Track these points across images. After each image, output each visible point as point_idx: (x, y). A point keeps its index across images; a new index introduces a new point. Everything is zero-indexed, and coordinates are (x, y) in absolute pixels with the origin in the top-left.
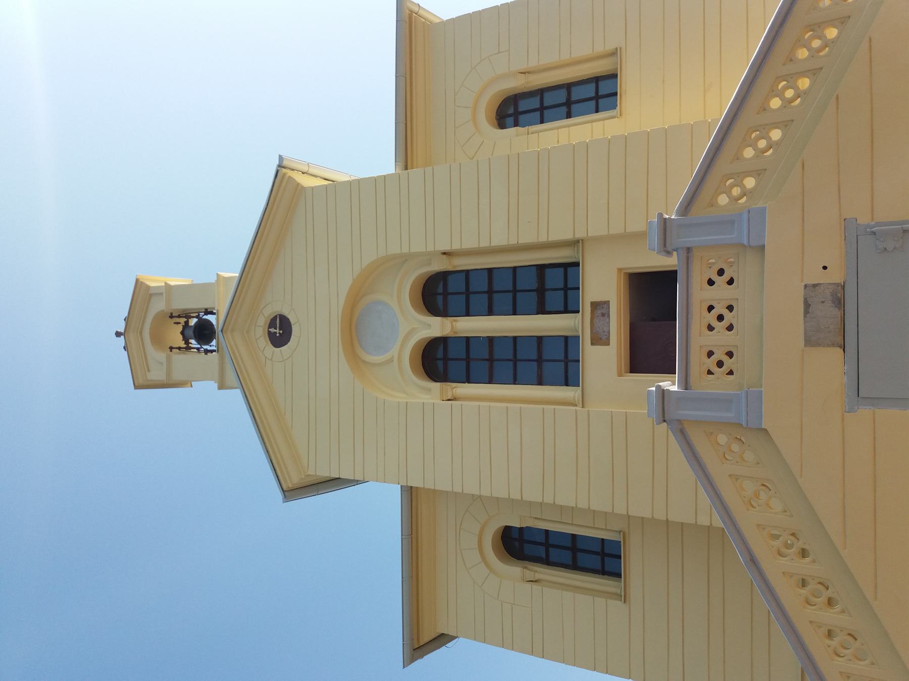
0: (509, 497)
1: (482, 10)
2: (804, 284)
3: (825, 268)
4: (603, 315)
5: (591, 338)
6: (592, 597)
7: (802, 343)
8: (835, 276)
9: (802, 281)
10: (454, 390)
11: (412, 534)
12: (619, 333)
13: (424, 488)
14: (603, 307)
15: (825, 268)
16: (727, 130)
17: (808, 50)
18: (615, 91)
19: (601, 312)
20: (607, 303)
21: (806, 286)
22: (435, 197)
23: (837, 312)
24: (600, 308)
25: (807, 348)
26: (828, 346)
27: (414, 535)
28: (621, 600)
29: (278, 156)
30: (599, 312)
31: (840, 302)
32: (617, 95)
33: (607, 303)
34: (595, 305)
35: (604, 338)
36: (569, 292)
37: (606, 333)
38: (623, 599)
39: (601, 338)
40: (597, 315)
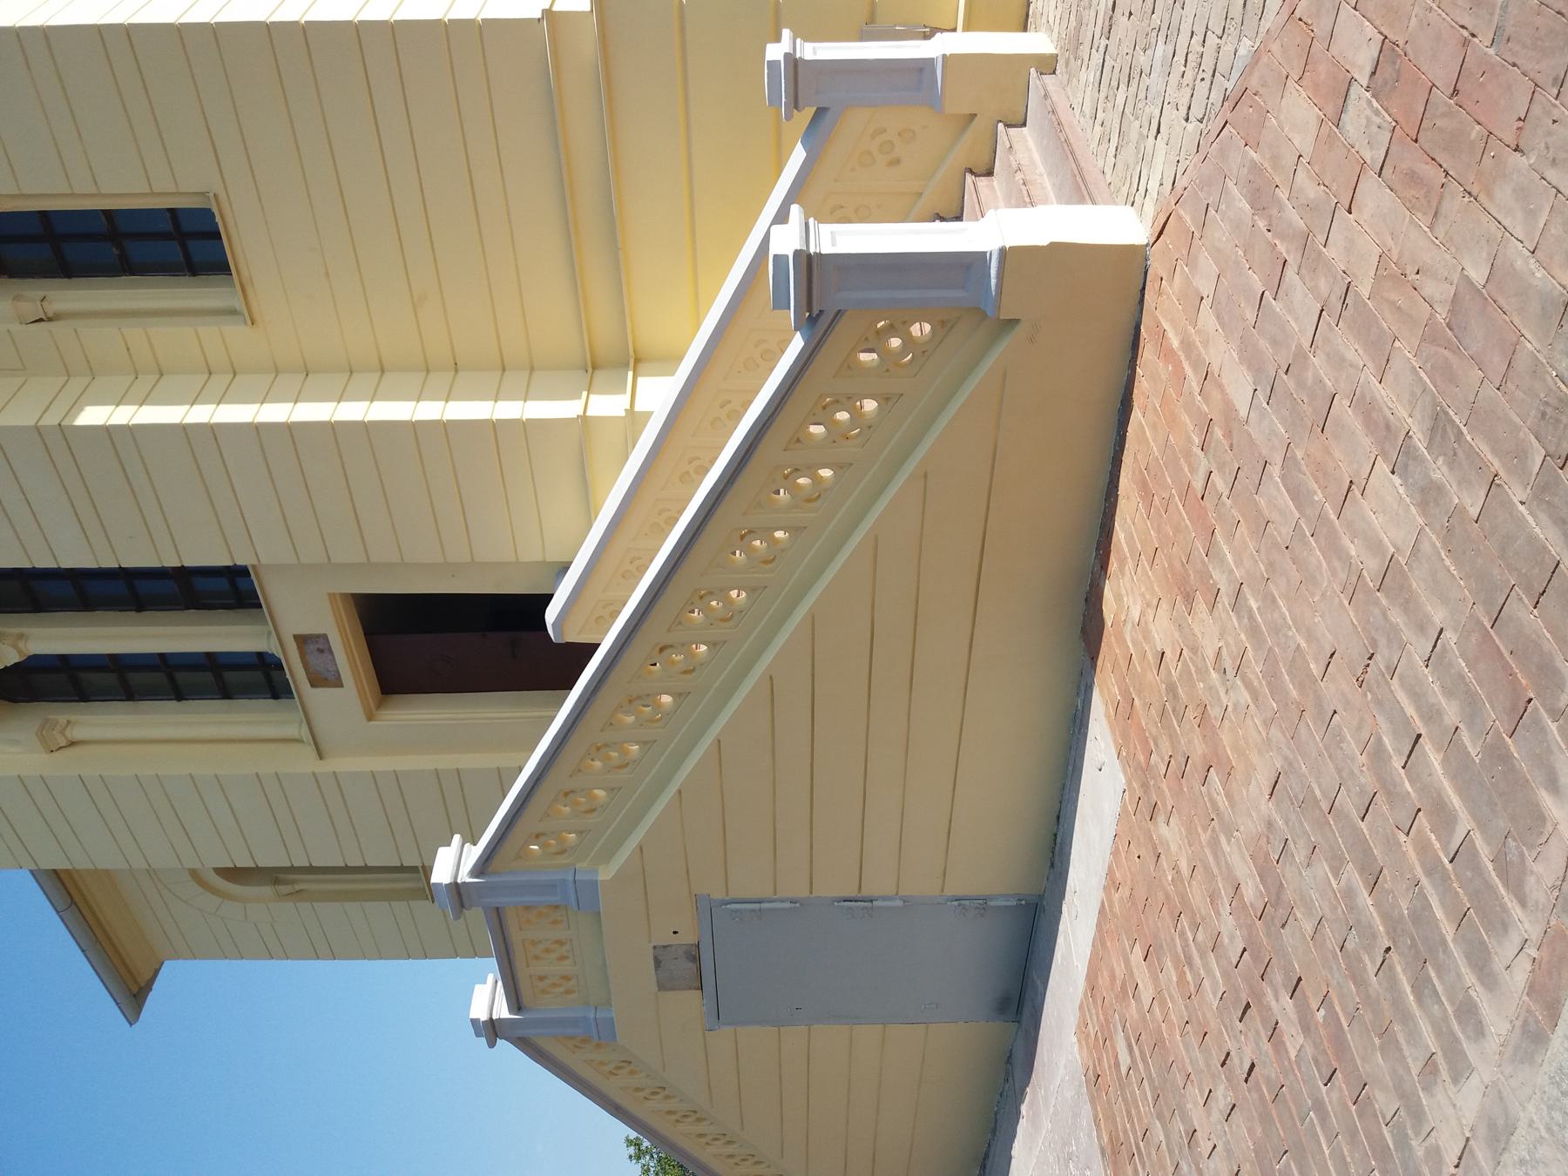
0: (402, 559)
2: (652, 945)
3: (675, 933)
6: (373, 559)
7: (655, 988)
8: (686, 937)
9: (650, 941)
10: (68, 733)
12: (353, 667)
15: (675, 933)
16: (615, 657)
17: (910, 334)
21: (655, 947)
23: (692, 966)
25: (660, 993)
26: (684, 989)
27: (77, 898)
28: (427, 899)
31: (695, 958)
38: (429, 897)
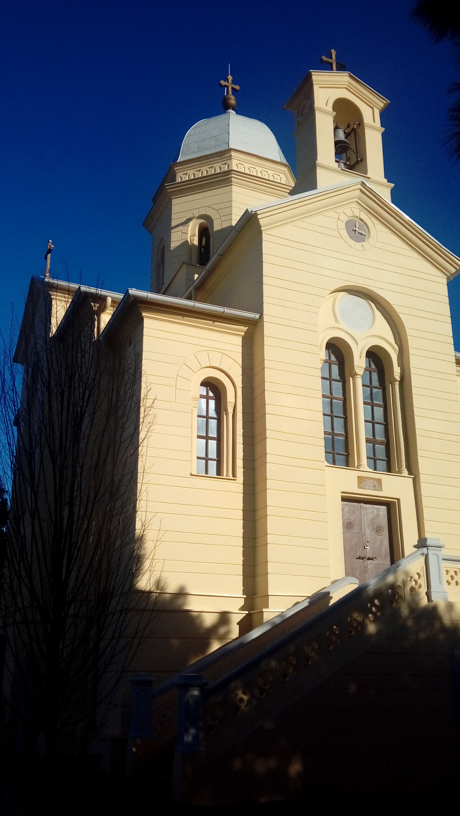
1: (243, 529)
4: (374, 486)
5: (362, 477)
11: (354, 249)
13: (267, 479)
14: (379, 486)
18: (378, 469)
19: (376, 485)
20: (381, 490)
22: (346, 215)
24: (378, 484)
29: (246, 209)
30: (376, 484)
32: (334, 465)
33: (381, 490)
34: (379, 481)
35: (362, 485)
36: (204, 455)
37: (364, 487)
39: (361, 483)
40: (374, 482)
